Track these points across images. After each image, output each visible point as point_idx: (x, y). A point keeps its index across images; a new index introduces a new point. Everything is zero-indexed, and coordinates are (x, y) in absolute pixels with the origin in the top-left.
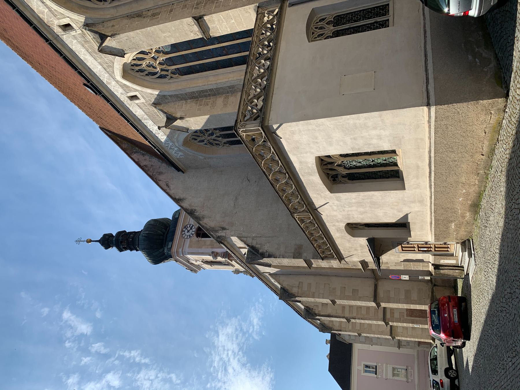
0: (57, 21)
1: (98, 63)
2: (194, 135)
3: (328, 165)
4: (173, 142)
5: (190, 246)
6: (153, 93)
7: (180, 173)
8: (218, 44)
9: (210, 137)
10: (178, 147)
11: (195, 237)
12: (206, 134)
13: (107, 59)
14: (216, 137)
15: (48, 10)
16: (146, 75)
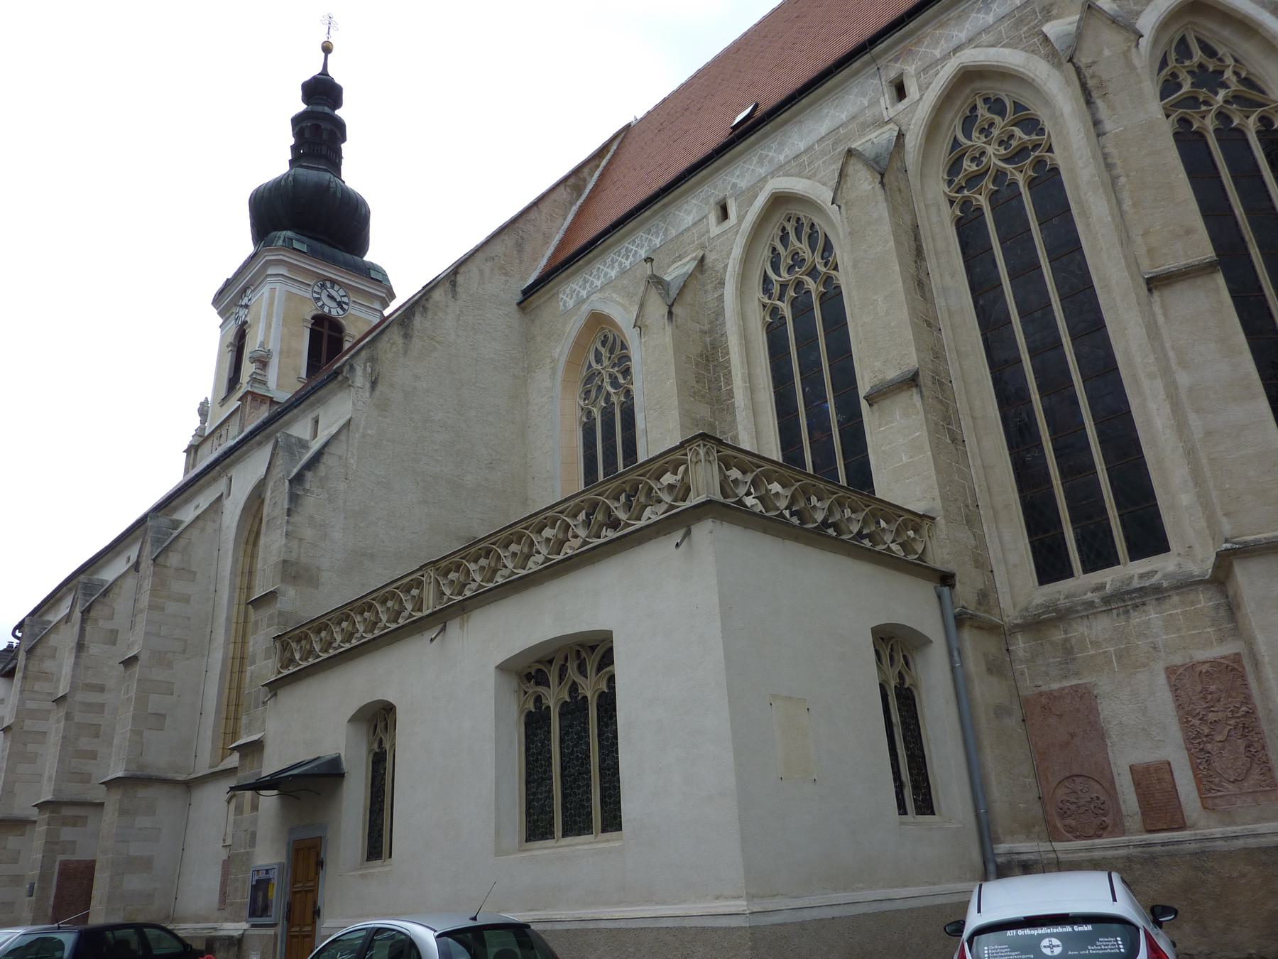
0: (913, 72)
1: (811, 143)
2: (615, 338)
3: (577, 662)
4: (601, 288)
5: (290, 296)
6: (731, 259)
7: (519, 297)
8: (838, 421)
9: (607, 380)
10: (588, 297)
11: (315, 312)
12: (616, 369)
13: (819, 166)
14: (608, 394)
15: (939, 57)
16: (774, 249)
